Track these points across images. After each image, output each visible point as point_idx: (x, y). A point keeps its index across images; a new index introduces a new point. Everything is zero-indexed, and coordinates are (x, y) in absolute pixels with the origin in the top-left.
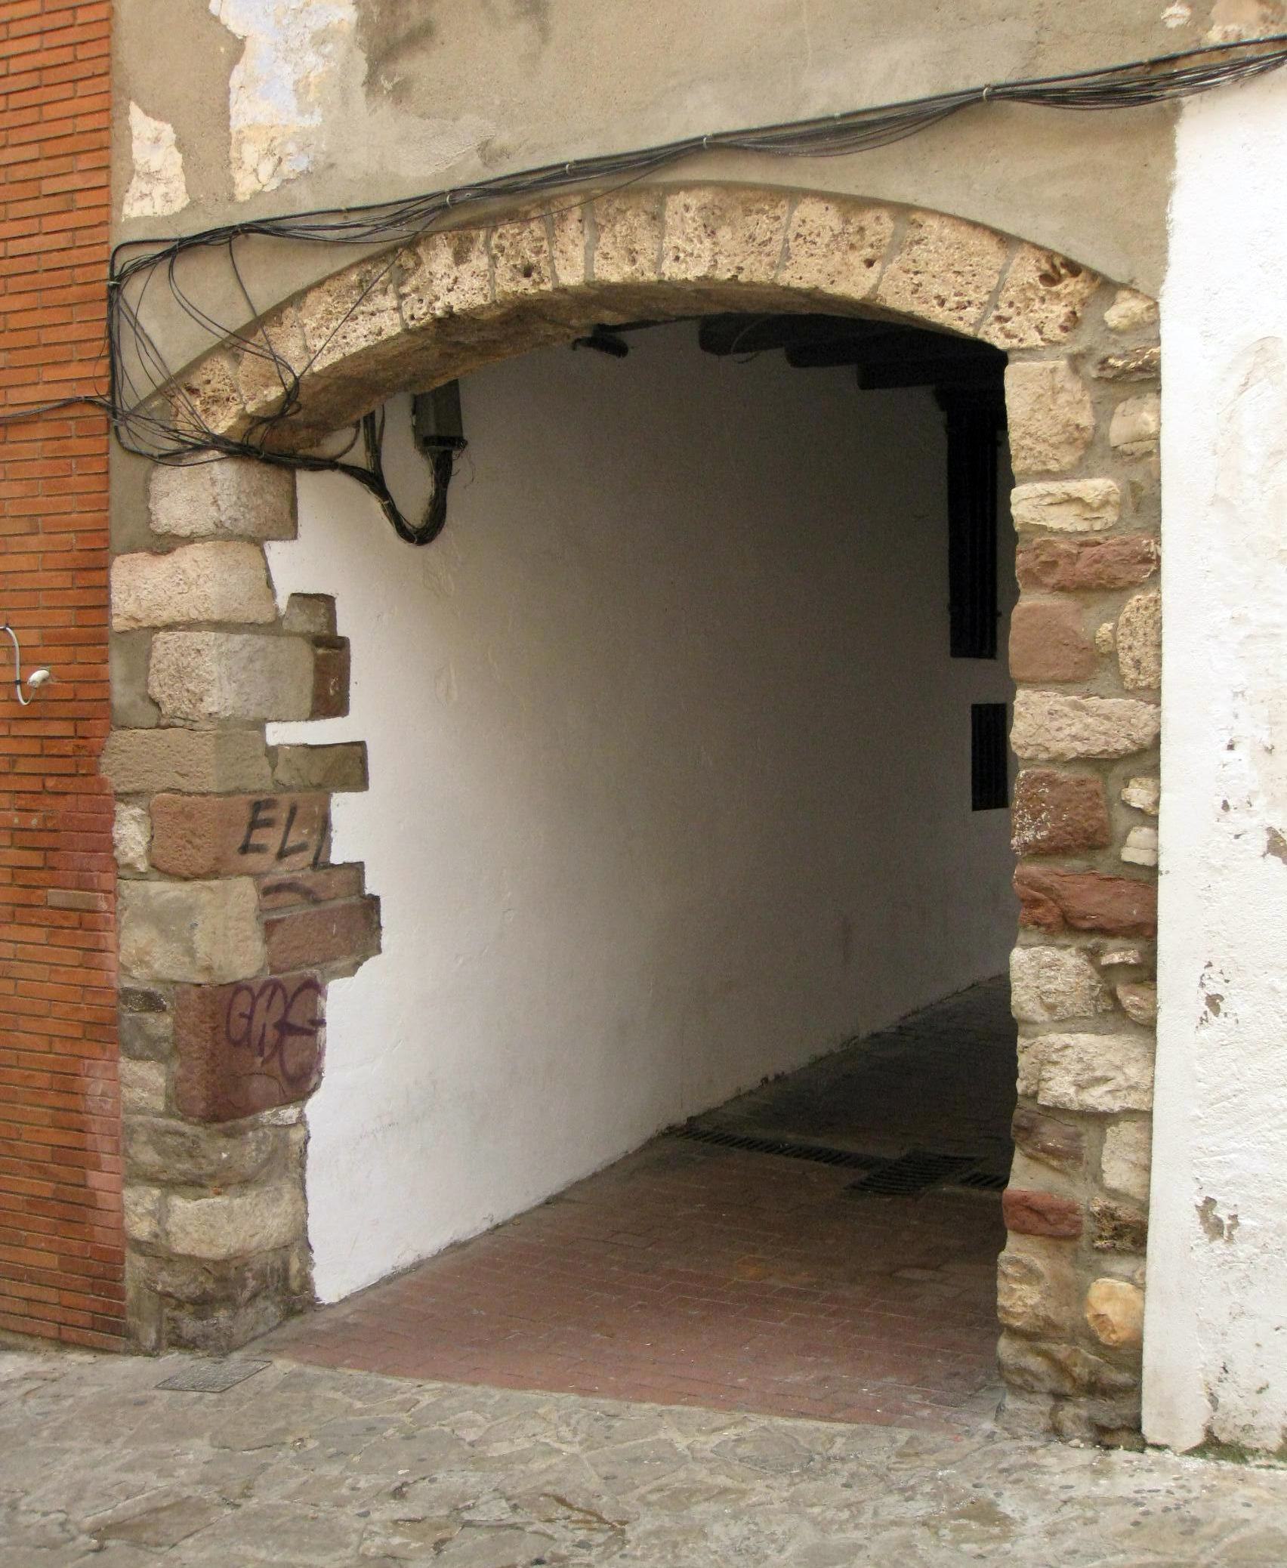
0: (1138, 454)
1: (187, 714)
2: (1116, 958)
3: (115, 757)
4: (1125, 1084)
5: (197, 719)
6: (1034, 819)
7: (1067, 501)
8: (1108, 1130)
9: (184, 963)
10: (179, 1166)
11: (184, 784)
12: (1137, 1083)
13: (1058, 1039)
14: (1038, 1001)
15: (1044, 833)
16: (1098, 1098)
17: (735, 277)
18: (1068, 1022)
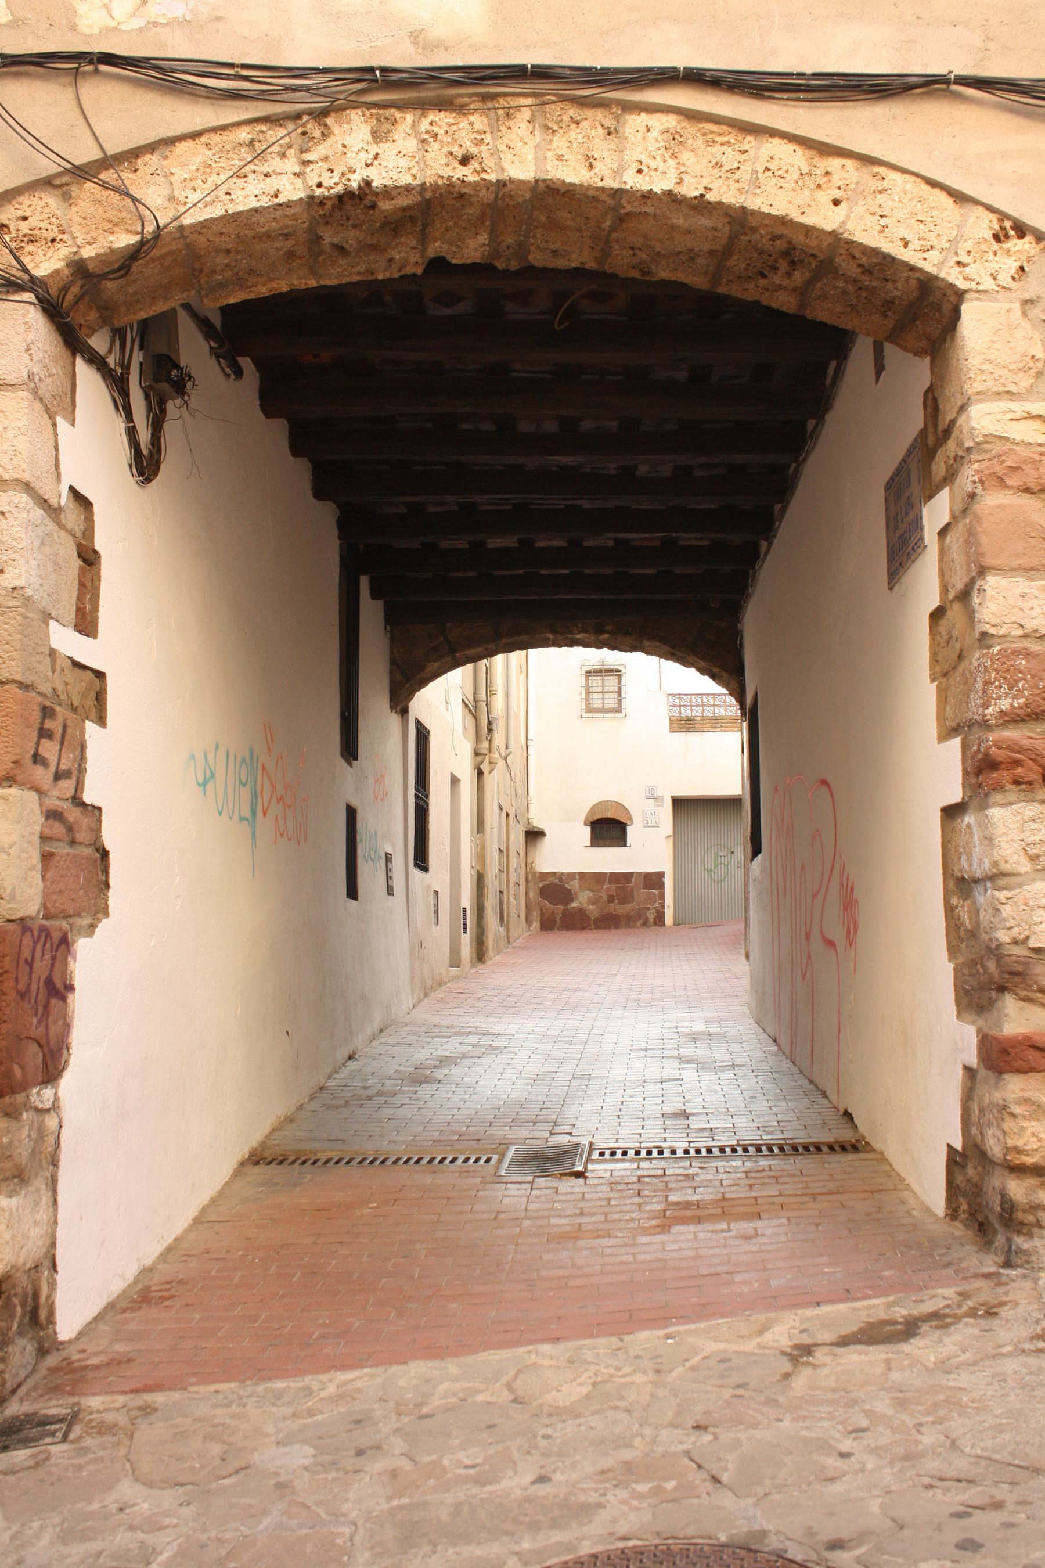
6: (1010, 688)
7: (1025, 418)
14: (1022, 853)
15: (1022, 701)
17: (702, 196)
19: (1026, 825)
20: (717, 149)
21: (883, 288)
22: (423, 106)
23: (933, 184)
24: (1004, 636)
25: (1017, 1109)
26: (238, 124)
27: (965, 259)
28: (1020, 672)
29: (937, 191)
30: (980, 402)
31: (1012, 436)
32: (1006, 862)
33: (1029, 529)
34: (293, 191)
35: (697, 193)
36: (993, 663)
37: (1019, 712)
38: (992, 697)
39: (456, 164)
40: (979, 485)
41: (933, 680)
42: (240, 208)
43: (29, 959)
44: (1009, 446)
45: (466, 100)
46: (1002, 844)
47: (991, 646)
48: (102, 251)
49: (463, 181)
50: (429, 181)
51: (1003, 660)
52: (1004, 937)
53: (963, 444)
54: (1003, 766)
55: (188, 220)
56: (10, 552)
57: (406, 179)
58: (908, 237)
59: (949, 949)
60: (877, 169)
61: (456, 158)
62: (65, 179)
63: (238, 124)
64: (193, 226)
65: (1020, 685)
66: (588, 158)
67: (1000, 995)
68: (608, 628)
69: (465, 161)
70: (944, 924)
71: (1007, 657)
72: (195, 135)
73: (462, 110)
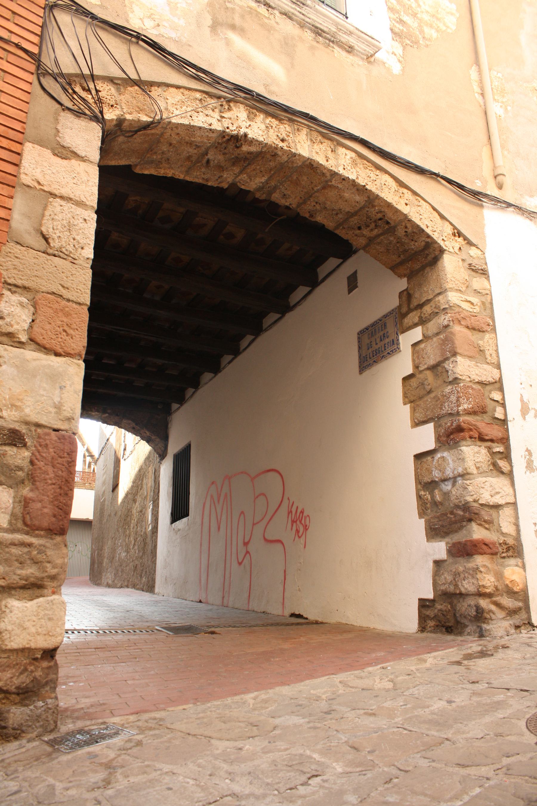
0: (484, 294)
1: (71, 252)
2: (498, 450)
3: (8, 259)
4: (505, 494)
5: (77, 258)
6: (467, 400)
9: (50, 412)
10: (19, 572)
11: (64, 292)
13: (481, 479)
15: (471, 406)
16: (498, 500)
17: (365, 186)
18: (482, 473)
20: (367, 171)
21: (409, 243)
22: (268, 114)
23: (434, 209)
25: (482, 569)
26: (196, 90)
27: (445, 239)
29: (435, 212)
31: (462, 306)
34: (217, 126)
35: (363, 184)
36: (461, 390)
37: (470, 410)
39: (279, 140)
40: (451, 322)
41: (405, 404)
42: (196, 124)
44: (461, 310)
45: (283, 118)
47: (460, 383)
48: (135, 119)
49: (282, 148)
50: (269, 143)
52: (469, 499)
53: (439, 307)
55: (174, 121)
56: (88, 240)
57: (261, 139)
58: (429, 225)
60: (417, 198)
61: (279, 138)
62: (119, 82)
63: (196, 90)
64: (175, 124)
66: (326, 157)
67: (469, 523)
68: (109, 411)
69: (283, 140)
72: (178, 87)
73: (280, 120)
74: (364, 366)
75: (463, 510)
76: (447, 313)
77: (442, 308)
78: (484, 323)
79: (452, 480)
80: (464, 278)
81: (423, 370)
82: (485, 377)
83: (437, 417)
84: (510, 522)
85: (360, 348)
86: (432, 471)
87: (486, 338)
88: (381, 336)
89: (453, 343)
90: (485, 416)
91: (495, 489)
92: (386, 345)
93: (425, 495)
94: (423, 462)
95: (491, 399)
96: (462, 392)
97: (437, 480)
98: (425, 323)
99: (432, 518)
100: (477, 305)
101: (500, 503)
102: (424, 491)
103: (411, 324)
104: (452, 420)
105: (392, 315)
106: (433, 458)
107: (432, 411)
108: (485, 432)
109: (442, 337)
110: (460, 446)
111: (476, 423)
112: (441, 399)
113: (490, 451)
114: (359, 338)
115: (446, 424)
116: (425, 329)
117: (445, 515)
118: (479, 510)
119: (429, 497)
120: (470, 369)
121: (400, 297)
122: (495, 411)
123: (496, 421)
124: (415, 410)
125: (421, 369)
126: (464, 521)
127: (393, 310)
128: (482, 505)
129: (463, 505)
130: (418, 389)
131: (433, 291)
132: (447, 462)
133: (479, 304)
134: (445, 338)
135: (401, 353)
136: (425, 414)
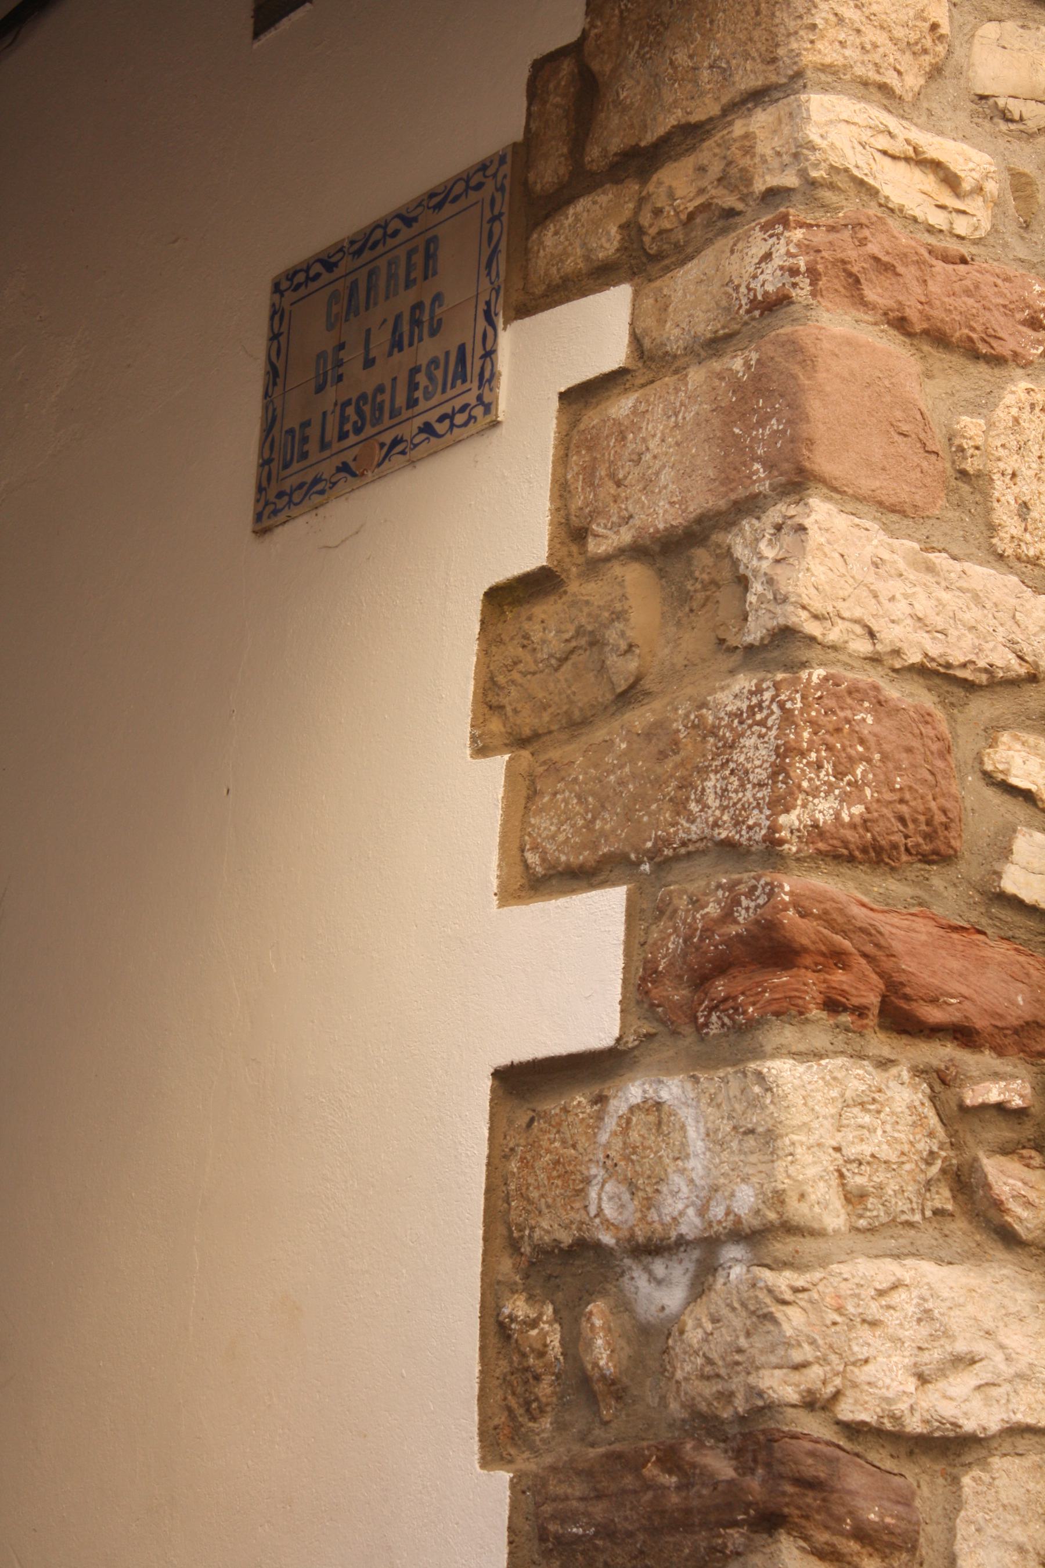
0: (1031, 125)
2: (994, 1093)
4: (1008, 1371)
6: (839, 775)
7: (907, 159)
8: (966, 1480)
12: (1031, 1365)
14: (835, 1181)
15: (858, 809)
19: (848, 1113)
24: (834, 648)
28: (862, 741)
30: (825, 89)
31: (886, 190)
32: (802, 1196)
33: (899, 414)
36: (806, 706)
37: (850, 835)
38: (799, 786)
40: (805, 282)
41: (482, 749)
43: (396, 350)
44: (873, 210)
46: (799, 1150)
47: (804, 665)
51: (832, 703)
54: (808, 960)
59: (482, 1434)
65: (859, 772)
67: (760, 1538)
70: (477, 1368)
71: (837, 697)
74: (286, 486)
75: (738, 1453)
76: (784, 221)
77: (759, 186)
78: (1008, 310)
79: (696, 1254)
80: (920, 16)
81: (607, 559)
82: (969, 640)
83: (652, 855)
84: (1021, 1549)
85: (274, 374)
86: (587, 1181)
87: (1009, 399)
88: (399, 318)
89: (797, 414)
90: (938, 878)
91: (948, 1334)
92: (422, 379)
93: (534, 1323)
94: (545, 1116)
95: (988, 777)
96: (812, 723)
97: (607, 1239)
98: (654, 269)
99: (553, 1469)
100: (979, 190)
101: (969, 1426)
102: (531, 1299)
103: (574, 263)
104: (732, 887)
105: (473, 196)
106: (601, 1100)
107: (628, 816)
108: (925, 977)
109: (738, 364)
110: (759, 1054)
111: (881, 921)
112: (688, 748)
113: (949, 1096)
114: (276, 313)
115: (696, 903)
116: (648, 302)
117: (632, 1462)
118: (831, 1461)
119: (555, 1341)
120: (879, 586)
121: (534, 91)
122: (1006, 853)
123: (1007, 915)
124: (533, 794)
125: (596, 547)
126: (735, 1524)
127: (483, 167)
128: (854, 1430)
129: (742, 1419)
130: (567, 666)
131: (726, 75)
132: (676, 1136)
133: (991, 187)
134: (757, 378)
135: (498, 432)
136: (589, 824)
